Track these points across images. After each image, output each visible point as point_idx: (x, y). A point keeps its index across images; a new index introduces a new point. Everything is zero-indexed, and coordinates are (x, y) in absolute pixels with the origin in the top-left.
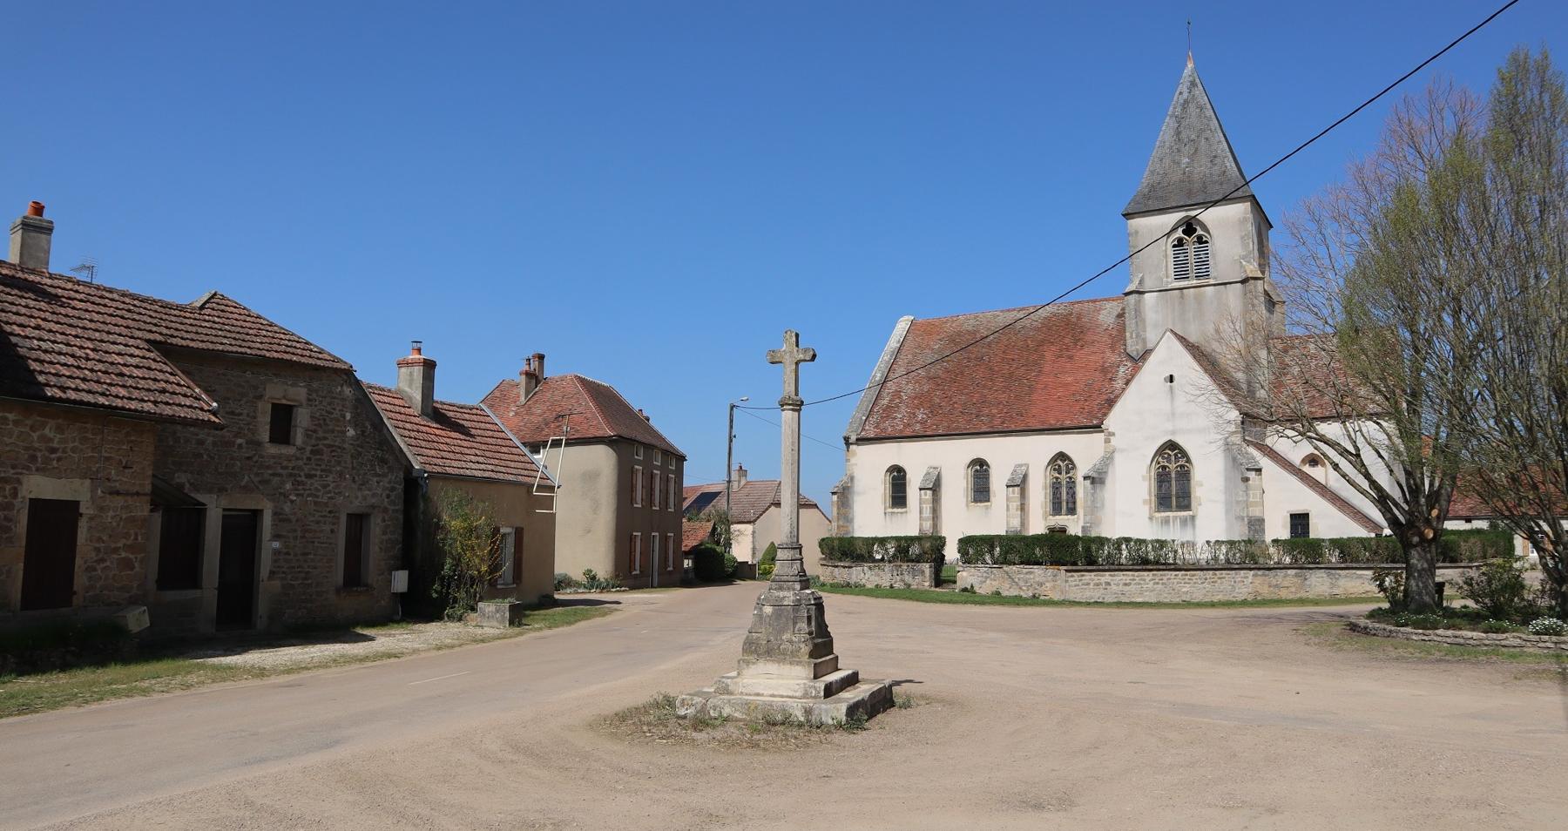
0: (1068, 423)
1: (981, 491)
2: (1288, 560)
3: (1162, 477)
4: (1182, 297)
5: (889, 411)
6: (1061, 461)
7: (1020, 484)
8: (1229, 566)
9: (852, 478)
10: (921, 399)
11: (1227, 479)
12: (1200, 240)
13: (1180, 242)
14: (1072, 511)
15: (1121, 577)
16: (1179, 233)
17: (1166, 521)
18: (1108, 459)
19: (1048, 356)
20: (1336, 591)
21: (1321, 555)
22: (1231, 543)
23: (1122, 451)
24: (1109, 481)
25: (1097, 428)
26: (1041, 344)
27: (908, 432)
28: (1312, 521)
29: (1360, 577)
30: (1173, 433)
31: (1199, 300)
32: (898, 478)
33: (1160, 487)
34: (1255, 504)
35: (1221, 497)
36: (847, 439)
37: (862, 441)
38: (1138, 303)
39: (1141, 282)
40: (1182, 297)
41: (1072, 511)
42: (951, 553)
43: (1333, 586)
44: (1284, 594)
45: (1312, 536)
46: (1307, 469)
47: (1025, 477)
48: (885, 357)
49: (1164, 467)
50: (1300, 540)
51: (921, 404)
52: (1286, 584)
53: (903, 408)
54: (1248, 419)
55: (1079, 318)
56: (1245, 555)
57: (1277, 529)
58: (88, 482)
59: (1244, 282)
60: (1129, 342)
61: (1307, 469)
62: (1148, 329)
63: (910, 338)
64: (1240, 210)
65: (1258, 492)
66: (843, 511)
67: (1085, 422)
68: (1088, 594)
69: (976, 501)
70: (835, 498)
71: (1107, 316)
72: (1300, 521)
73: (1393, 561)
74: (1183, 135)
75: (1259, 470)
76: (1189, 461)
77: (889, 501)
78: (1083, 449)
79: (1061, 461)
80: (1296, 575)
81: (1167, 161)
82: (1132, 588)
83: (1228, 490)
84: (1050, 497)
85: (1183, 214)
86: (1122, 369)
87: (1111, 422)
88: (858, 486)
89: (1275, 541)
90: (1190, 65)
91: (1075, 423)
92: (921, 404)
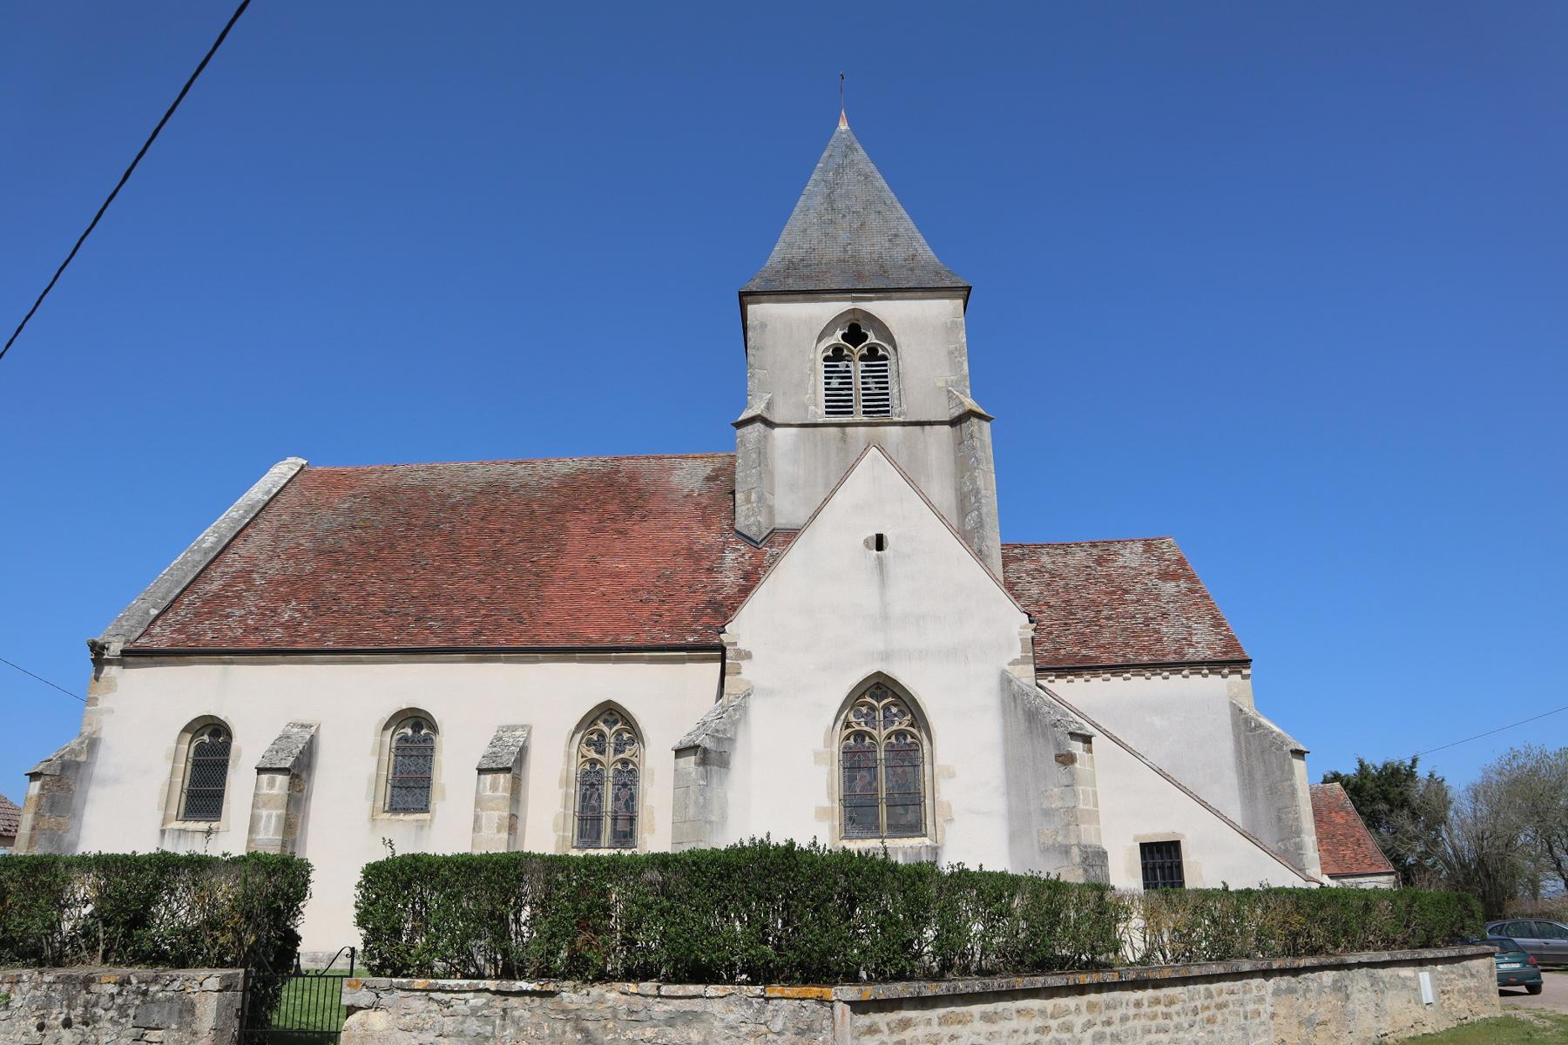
0: (628, 639)
1: (410, 784)
4: (844, 439)
5: (215, 605)
6: (609, 723)
9: (93, 744)
10: (292, 587)
12: (872, 354)
13: (837, 354)
16: (837, 338)
23: (769, 693)
24: (737, 761)
26: (559, 510)
27: (253, 642)
30: (886, 656)
32: (210, 745)
35: (999, 804)
36: (98, 650)
37: (135, 655)
39: (769, 406)
40: (844, 439)
42: (328, 927)
47: (523, 752)
48: (236, 512)
49: (860, 735)
53: (251, 601)
59: (954, 422)
60: (741, 509)
62: (779, 490)
63: (292, 490)
66: (49, 821)
67: (667, 638)
69: (394, 809)
70: (35, 787)
71: (689, 475)
73: (1297, 955)
74: (839, 205)
75: (1087, 740)
77: (178, 800)
79: (609, 723)
81: (815, 233)
84: (574, 805)
85: (846, 306)
86: (730, 556)
88: (106, 762)
90: (843, 126)
91: (645, 639)
92: (294, 594)
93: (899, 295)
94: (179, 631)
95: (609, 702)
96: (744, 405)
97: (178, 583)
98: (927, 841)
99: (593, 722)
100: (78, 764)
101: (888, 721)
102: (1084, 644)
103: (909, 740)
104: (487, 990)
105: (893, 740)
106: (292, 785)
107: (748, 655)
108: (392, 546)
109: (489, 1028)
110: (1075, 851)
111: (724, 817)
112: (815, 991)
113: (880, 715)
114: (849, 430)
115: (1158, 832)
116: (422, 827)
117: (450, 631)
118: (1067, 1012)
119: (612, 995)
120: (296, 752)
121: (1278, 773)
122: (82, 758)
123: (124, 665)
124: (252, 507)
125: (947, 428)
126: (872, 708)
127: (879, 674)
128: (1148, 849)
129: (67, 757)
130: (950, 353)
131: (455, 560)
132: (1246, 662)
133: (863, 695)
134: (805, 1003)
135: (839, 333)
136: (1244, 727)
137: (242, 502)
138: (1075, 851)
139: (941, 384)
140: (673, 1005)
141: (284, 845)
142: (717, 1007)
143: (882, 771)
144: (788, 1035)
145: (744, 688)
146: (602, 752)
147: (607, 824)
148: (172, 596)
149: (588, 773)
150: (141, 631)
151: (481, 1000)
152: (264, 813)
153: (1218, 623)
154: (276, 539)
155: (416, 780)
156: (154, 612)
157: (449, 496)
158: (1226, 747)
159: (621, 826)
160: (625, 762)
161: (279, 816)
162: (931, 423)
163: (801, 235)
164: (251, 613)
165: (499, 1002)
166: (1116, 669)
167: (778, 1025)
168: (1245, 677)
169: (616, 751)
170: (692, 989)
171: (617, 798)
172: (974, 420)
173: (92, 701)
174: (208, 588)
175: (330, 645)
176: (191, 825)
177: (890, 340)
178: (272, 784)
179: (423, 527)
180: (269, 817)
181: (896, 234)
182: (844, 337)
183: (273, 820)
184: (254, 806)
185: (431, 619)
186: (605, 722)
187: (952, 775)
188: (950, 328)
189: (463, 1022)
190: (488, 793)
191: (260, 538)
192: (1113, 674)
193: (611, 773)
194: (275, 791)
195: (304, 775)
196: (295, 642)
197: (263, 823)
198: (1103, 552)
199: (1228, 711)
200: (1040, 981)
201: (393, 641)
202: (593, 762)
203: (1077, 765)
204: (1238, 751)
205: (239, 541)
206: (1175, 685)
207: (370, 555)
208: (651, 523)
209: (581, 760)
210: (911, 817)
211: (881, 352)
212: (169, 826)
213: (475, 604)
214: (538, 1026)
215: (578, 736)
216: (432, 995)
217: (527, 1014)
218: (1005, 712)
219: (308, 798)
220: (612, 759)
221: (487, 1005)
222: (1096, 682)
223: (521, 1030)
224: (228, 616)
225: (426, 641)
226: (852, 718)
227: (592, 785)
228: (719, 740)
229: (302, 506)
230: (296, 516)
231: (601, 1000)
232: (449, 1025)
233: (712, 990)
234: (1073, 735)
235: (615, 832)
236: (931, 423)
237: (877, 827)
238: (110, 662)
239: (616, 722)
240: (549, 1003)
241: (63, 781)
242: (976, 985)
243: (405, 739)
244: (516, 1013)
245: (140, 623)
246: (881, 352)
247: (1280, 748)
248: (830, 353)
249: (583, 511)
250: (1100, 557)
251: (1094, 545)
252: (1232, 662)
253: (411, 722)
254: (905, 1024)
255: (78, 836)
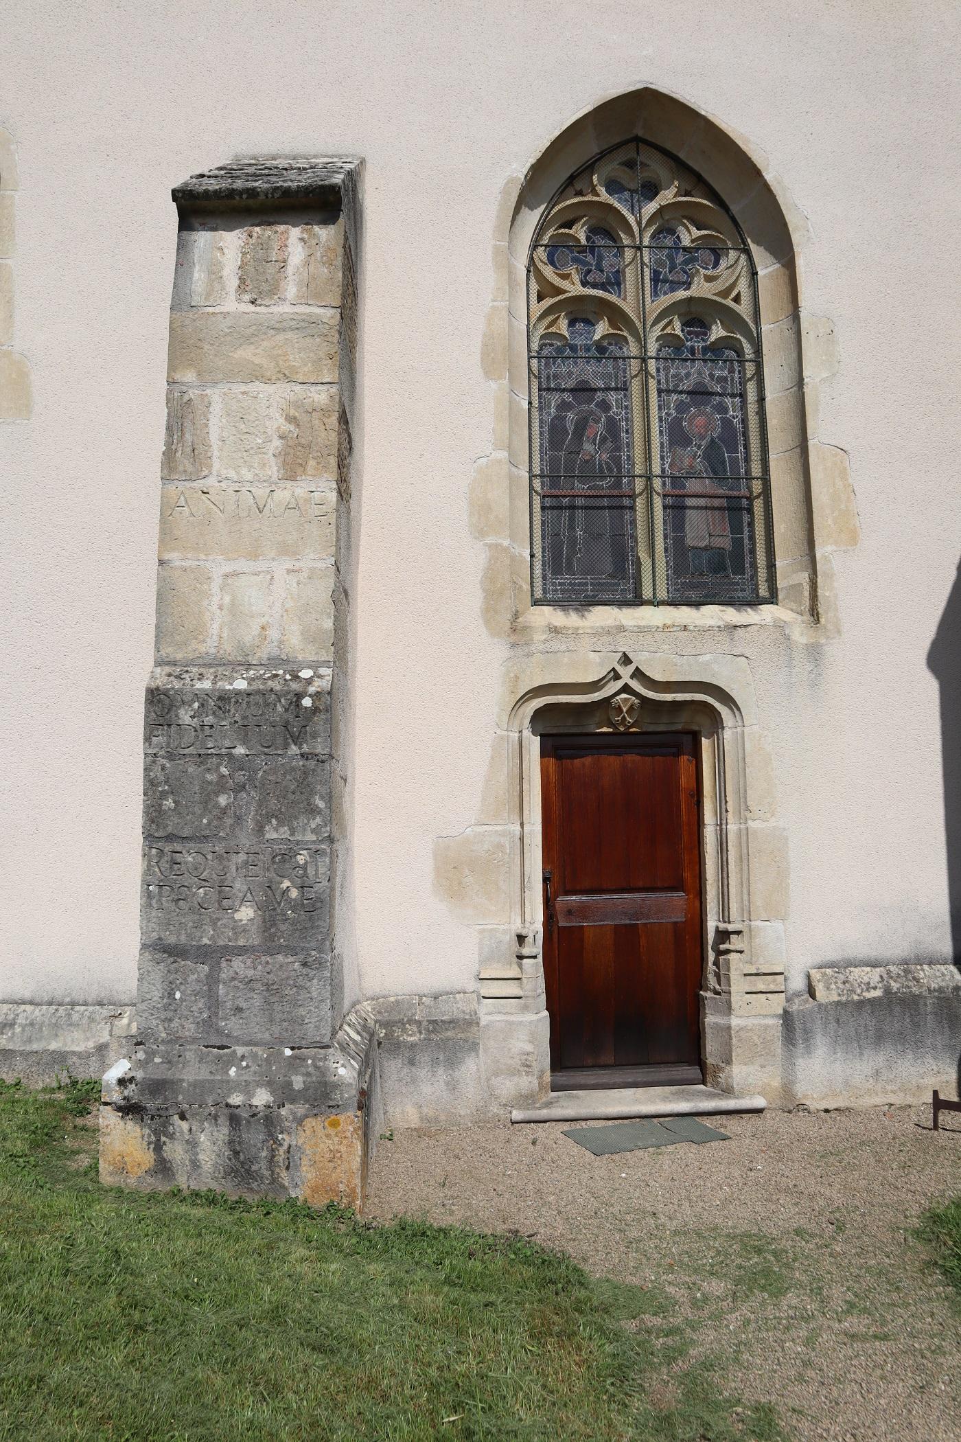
95: (646, 89)
147: (650, 525)
159: (702, 529)
160: (696, 315)
171: (677, 436)
184: (167, 534)
186: (613, 187)
190: (232, 304)
200: (680, 697)
215: (531, 218)
235: (679, 552)
239: (651, 190)
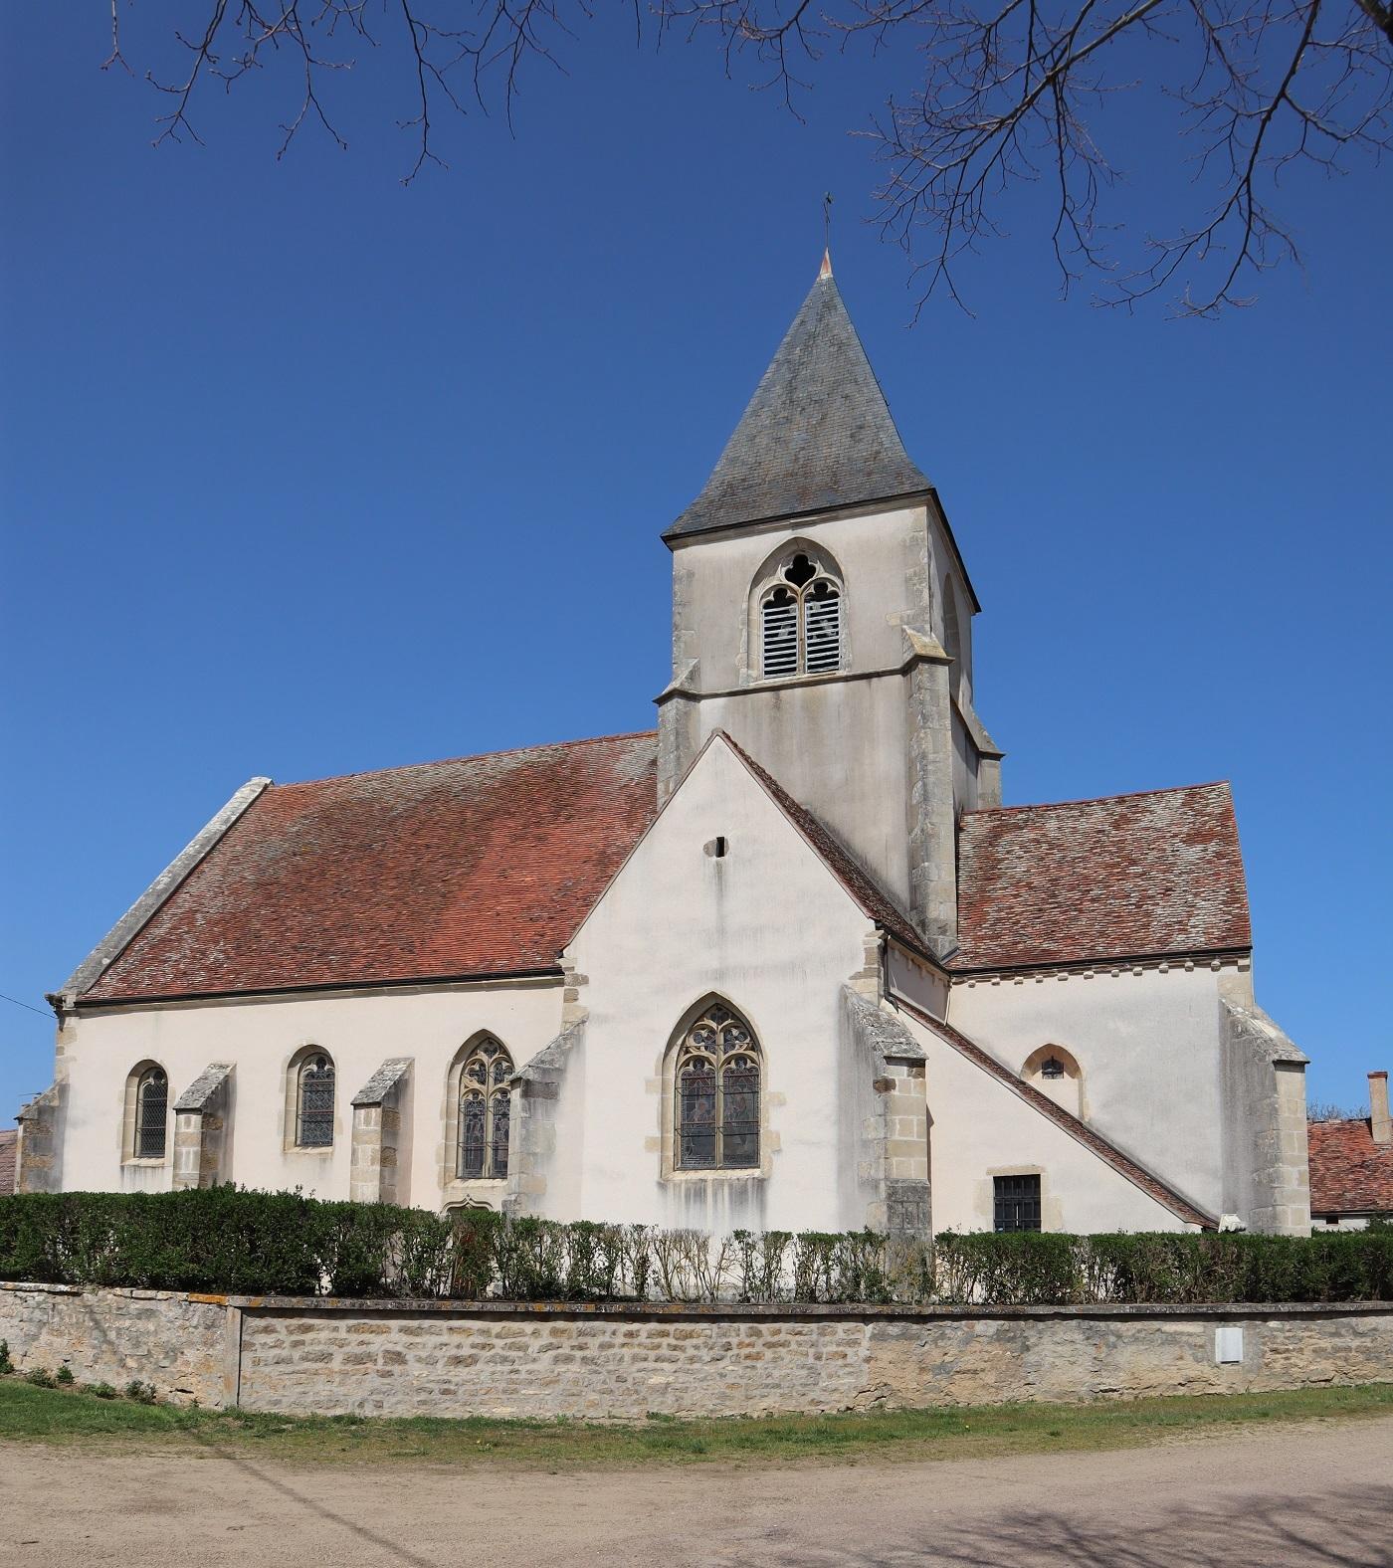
0: (501, 964)
2: (979, 1293)
3: (694, 1086)
4: (777, 706)
7: (390, 1101)
8: (805, 1309)
9: (63, 1090)
11: (844, 1088)
13: (780, 598)
14: (501, 1170)
15: (440, 1337)
16: (780, 577)
17: (697, 1193)
18: (572, 1036)
19: (499, 837)
20: (1109, 1382)
21: (1069, 1280)
22: (817, 1242)
23: (604, 1019)
24: (567, 1092)
25: (552, 974)
27: (178, 989)
28: (1048, 1194)
29: (1172, 1340)
30: (721, 975)
31: (812, 712)
33: (688, 1109)
34: (905, 1148)
35: (828, 1133)
36: (56, 1002)
37: (89, 1006)
38: (684, 718)
39: (693, 675)
40: (777, 706)
41: (501, 1170)
43: (1099, 1366)
44: (965, 1393)
45: (1048, 1225)
46: (1038, 1081)
48: (192, 849)
49: (699, 1061)
50: (1014, 1238)
51: (223, 934)
52: (969, 1361)
54: (902, 943)
55: (576, 770)
56: (861, 1283)
57: (964, 1208)
58: (411, 1208)
59: (906, 670)
61: (1038, 1081)
63: (252, 816)
64: (907, 522)
65: (917, 1120)
66: (35, 1160)
68: (322, 1389)
72: (1017, 1194)
73: (1251, 1297)
75: (918, 1064)
76: (755, 1045)
78: (522, 1019)
80: (999, 1337)
81: (763, 441)
82: (483, 1371)
83: (846, 1114)
87: (579, 954)
88: (77, 1105)
89: (946, 1238)
90: (825, 274)
91: (518, 963)
93: (846, 512)
94: (123, 980)
96: (670, 677)
97: (132, 929)
98: (757, 1173)
99: (474, 1052)
100: (53, 1108)
101: (729, 1044)
102: (1049, 935)
103: (749, 1064)
104: (43, 1291)
105: (733, 1065)
106: (204, 1124)
107: (584, 980)
108: (323, 873)
109: (46, 1317)
110: (882, 1185)
111: (550, 1149)
112: (217, 1298)
113: (721, 1038)
114: (783, 692)
115: (1015, 1164)
116: (324, 1161)
117: (345, 965)
118: (522, 1333)
119: (110, 1296)
120: (208, 1092)
121: (1258, 1089)
122: (55, 1103)
123: (80, 1016)
124: (209, 839)
125: (899, 677)
126: (712, 1031)
127: (713, 994)
128: (1003, 1183)
129: (42, 1103)
130: (908, 580)
131: (374, 885)
132: (1245, 950)
133: (700, 1018)
134: (211, 1307)
135: (781, 572)
136: (1233, 1032)
137: (202, 834)
138: (882, 1185)
139: (894, 622)
140: (141, 1305)
141: (202, 1178)
142: (163, 1307)
143: (720, 1099)
144: (201, 1329)
145: (580, 1015)
146: (483, 1083)
148: (124, 943)
149: (470, 1104)
150: (93, 981)
151: (40, 1297)
152: (184, 1150)
153: (1234, 897)
154: (226, 873)
155: (323, 1115)
156: (106, 962)
157: (392, 809)
158: (1209, 1058)
161: (195, 1153)
162: (878, 675)
163: (754, 444)
164: (185, 957)
165: (51, 1299)
166: (1075, 966)
167: (195, 1322)
168: (1242, 969)
169: (497, 1081)
170: (150, 1293)
172: (924, 667)
173: (60, 1050)
174: (157, 931)
175: (239, 986)
176: (145, 1162)
177: (838, 573)
178: (188, 1123)
179: (357, 849)
180: (188, 1153)
181: (867, 424)
182: (789, 575)
183: (191, 1156)
185: (333, 954)
187: (782, 1103)
188: (909, 547)
189: (32, 1312)
190: (363, 1127)
191: (212, 873)
192: (1071, 972)
193: (491, 1103)
194: (191, 1130)
195: (220, 1113)
196: (212, 985)
197: (184, 1159)
198: (1130, 805)
199: (1215, 1011)
201: (293, 979)
202: (476, 1093)
203: (895, 1093)
204: (1223, 1062)
205: (193, 879)
206: (1151, 981)
207: (300, 885)
208: (576, 824)
209: (463, 1091)
210: (747, 1147)
211: (830, 588)
212: (127, 1163)
213: (376, 933)
214: (70, 1316)
216: (18, 1293)
217: (65, 1308)
218: (841, 1033)
219: (229, 1134)
220: (492, 1088)
221: (44, 1302)
222: (1051, 982)
223: (62, 1319)
224: (165, 962)
225: (321, 976)
226: (691, 1042)
227: (475, 1116)
228: (545, 1071)
229: (256, 832)
230: (249, 845)
231: (104, 1299)
232: (26, 1314)
233: (161, 1295)
234: (890, 1059)
236: (878, 675)
237: (714, 1158)
238: (68, 1014)
239: (495, 1052)
240: (77, 1300)
241: (43, 1123)
242: (591, 1308)
243: (311, 1075)
244: (60, 1307)
245: (93, 974)
246: (830, 588)
247: (1262, 1059)
248: (771, 598)
249: (512, 815)
250: (1123, 816)
251: (1121, 800)
252: (1229, 951)
253: (315, 1058)
254: (308, 1329)
255: (62, 1173)
